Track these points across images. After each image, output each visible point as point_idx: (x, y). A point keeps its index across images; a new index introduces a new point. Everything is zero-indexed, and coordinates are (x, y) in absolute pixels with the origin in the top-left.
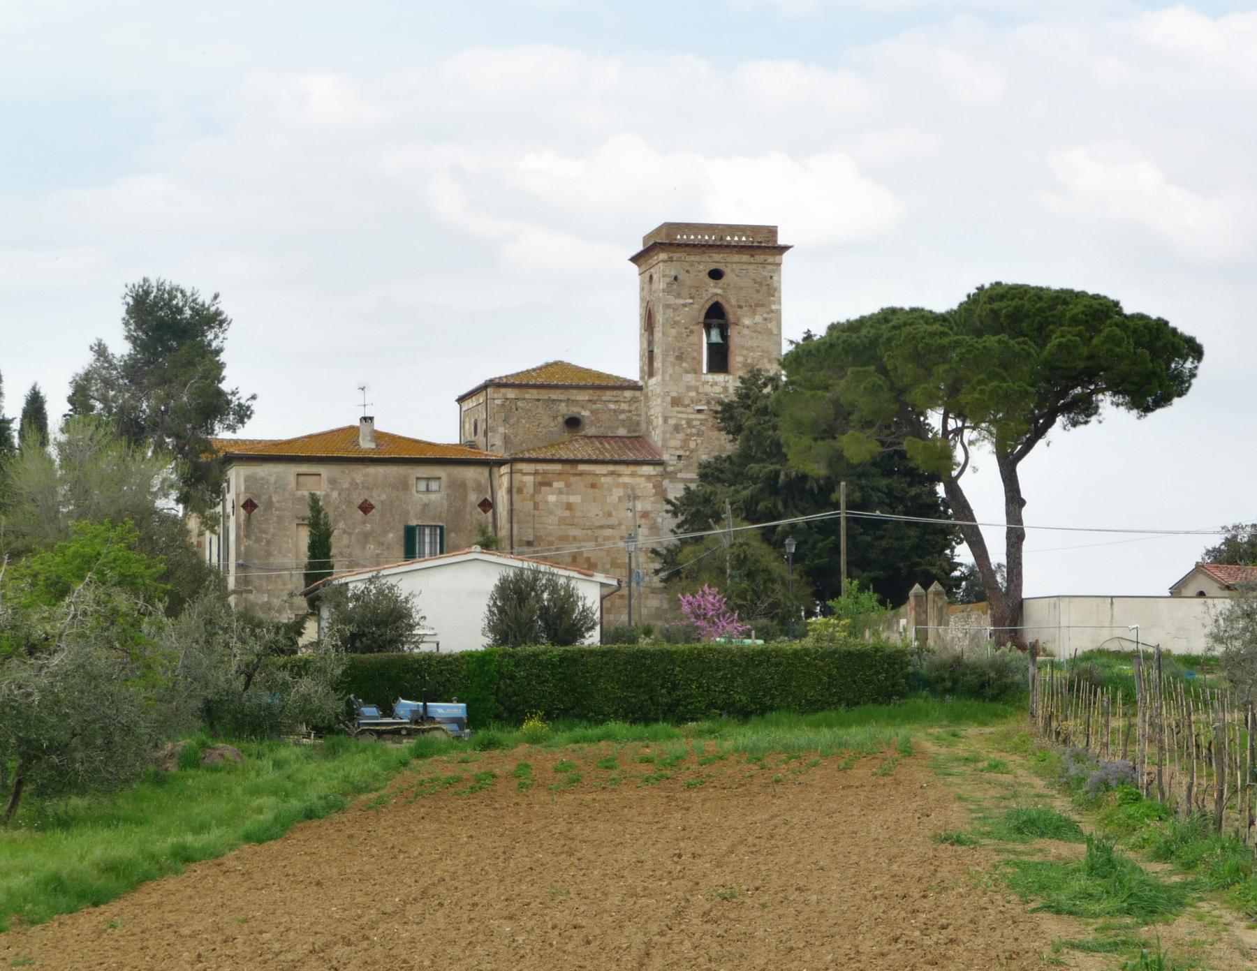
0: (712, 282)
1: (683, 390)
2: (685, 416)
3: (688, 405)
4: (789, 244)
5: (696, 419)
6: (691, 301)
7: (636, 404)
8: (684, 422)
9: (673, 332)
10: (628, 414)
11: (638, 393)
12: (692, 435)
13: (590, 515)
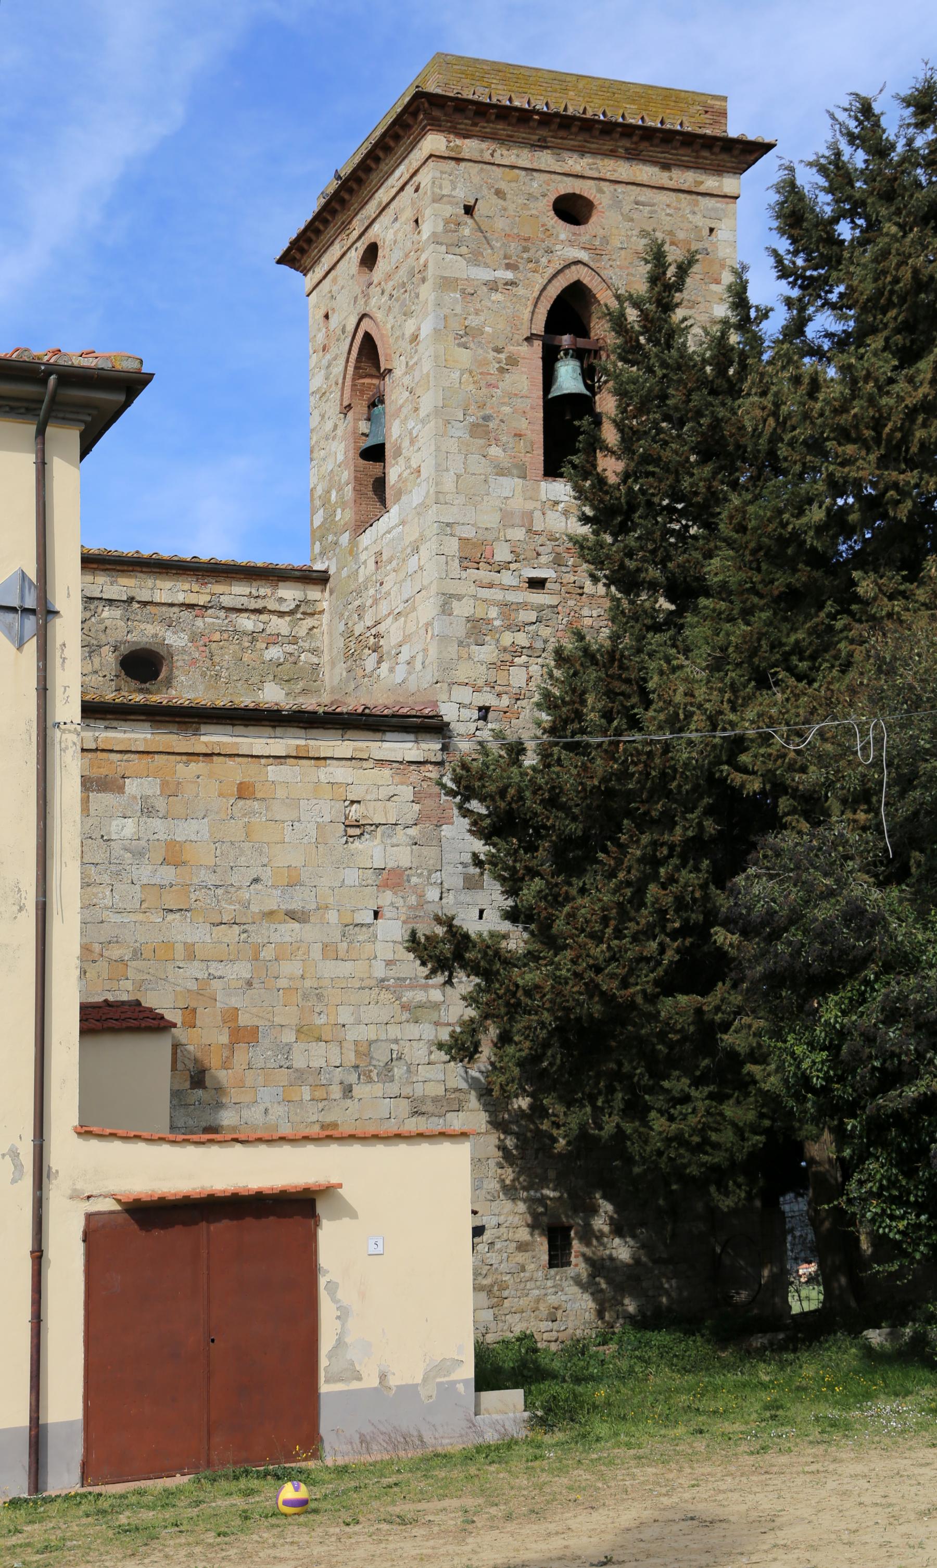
0: (563, 230)
1: (490, 519)
2: (496, 594)
3: (506, 565)
4: (768, 140)
5: (525, 605)
6: (509, 275)
7: (309, 622)
8: (493, 613)
9: (464, 357)
10: (290, 648)
11: (313, 593)
12: (517, 651)
13: (234, 879)
